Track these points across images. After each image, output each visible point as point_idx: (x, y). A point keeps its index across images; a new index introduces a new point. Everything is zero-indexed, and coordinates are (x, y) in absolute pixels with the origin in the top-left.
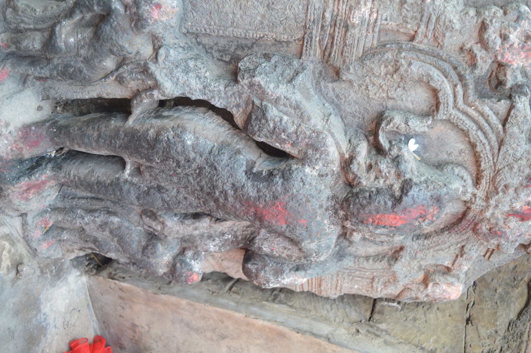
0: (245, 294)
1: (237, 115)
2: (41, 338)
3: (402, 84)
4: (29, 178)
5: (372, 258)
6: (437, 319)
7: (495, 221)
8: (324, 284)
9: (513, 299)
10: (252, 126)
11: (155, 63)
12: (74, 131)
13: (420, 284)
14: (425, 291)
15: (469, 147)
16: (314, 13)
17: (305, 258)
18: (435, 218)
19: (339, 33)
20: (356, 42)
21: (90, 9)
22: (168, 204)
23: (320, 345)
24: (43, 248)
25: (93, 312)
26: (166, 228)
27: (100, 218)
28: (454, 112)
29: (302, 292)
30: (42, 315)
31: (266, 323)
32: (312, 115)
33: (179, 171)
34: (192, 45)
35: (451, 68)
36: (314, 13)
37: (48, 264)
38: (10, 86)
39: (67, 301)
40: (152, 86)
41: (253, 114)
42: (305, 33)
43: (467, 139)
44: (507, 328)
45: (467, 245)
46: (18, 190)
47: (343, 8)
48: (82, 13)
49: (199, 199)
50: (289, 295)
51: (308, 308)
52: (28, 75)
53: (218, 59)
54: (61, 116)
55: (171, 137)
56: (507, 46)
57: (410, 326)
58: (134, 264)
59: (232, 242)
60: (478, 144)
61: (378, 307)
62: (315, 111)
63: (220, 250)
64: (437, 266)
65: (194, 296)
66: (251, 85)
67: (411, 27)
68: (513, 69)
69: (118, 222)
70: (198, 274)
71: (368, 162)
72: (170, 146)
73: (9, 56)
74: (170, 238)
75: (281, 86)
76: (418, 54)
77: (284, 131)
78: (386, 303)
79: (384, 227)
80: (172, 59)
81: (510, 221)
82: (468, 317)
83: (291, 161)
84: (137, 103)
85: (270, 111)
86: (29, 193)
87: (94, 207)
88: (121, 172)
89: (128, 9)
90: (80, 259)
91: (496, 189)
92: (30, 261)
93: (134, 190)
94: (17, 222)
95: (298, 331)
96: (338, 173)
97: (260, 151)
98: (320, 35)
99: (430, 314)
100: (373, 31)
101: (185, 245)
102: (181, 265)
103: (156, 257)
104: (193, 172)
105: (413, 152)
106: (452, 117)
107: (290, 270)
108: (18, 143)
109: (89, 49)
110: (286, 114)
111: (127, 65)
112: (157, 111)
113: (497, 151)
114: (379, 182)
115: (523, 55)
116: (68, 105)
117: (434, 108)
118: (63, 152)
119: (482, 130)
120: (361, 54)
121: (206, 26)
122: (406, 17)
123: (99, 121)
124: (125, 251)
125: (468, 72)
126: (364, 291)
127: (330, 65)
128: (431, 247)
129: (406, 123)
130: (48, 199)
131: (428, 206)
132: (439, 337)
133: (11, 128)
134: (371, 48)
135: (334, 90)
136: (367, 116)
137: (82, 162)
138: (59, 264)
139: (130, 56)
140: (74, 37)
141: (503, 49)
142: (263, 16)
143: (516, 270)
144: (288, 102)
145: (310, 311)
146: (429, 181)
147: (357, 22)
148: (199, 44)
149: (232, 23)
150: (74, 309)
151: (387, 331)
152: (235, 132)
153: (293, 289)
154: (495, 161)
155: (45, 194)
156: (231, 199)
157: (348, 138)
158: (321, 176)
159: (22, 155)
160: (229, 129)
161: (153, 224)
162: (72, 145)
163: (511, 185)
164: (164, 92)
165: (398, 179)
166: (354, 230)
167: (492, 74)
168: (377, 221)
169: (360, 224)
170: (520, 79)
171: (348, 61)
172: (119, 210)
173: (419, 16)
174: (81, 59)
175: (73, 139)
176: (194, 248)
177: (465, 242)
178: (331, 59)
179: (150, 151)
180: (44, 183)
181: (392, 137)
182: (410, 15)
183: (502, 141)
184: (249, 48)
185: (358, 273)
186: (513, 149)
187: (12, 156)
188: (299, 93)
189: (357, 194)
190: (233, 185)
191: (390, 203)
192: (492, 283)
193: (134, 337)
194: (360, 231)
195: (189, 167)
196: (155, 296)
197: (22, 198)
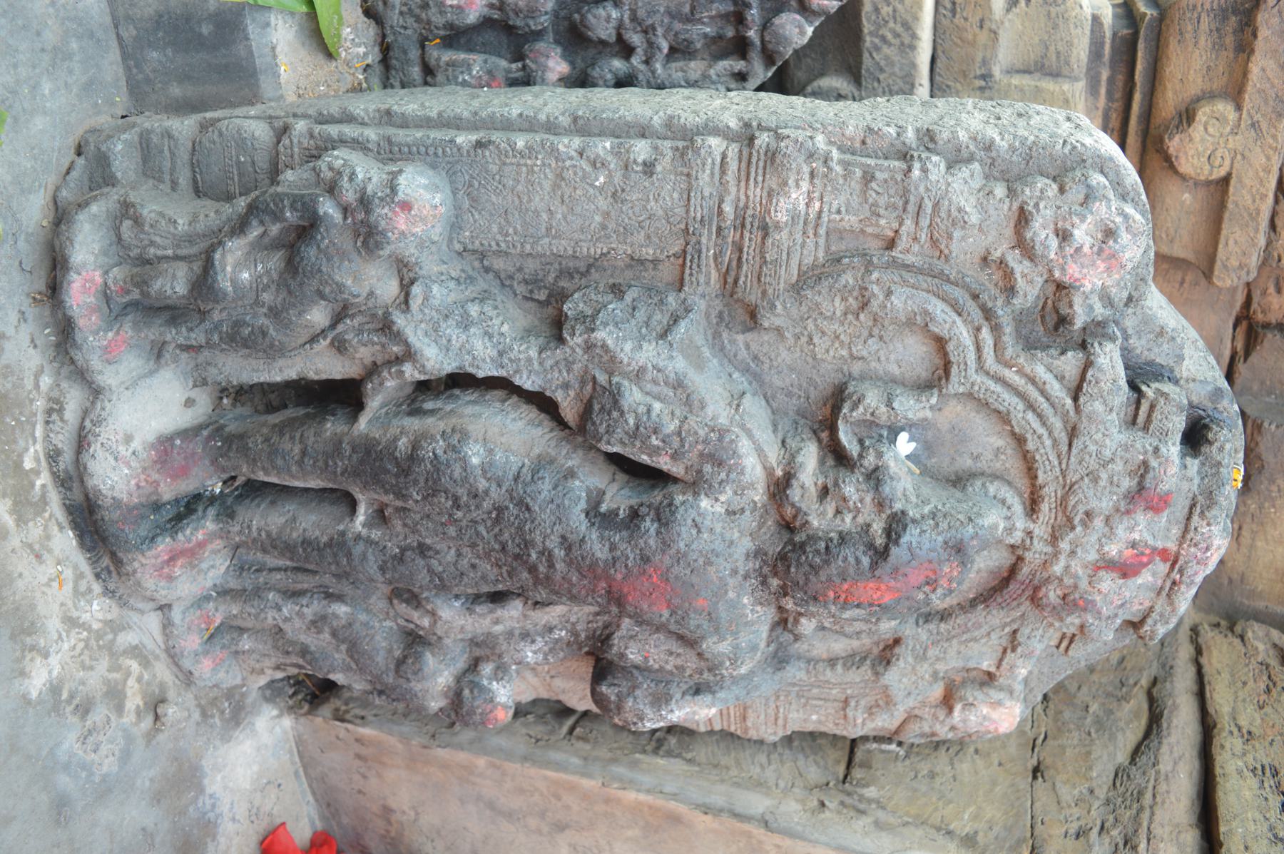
0: (600, 740)
1: (565, 404)
2: (206, 844)
3: (876, 331)
4: (172, 537)
5: (841, 662)
6: (976, 773)
9: (1122, 724)
10: (594, 424)
11: (403, 312)
12: (256, 443)
13: (936, 706)
14: (948, 720)
15: (1013, 444)
17: (710, 670)
19: (750, 240)
20: (784, 256)
21: (277, 216)
22: (441, 579)
23: (749, 835)
24: (204, 669)
25: (306, 785)
27: (313, 608)
28: (979, 379)
29: (711, 733)
30: (207, 798)
31: (642, 797)
32: (707, 397)
33: (459, 514)
34: (475, 274)
35: (967, 296)
37: (216, 698)
38: (133, 365)
39: (255, 768)
40: (400, 354)
42: (687, 244)
44: (1111, 782)
46: (153, 561)
47: (756, 193)
49: (500, 567)
50: (687, 738)
52: (164, 343)
53: (525, 298)
54: (231, 416)
55: (439, 452)
56: (1069, 250)
57: (924, 788)
58: (381, 693)
59: (569, 644)
60: (1029, 436)
61: (859, 755)
62: (714, 390)
64: (968, 670)
65: (501, 750)
66: (589, 347)
67: (886, 224)
69: (346, 613)
70: (505, 707)
71: (820, 482)
72: (438, 470)
73: (129, 309)
74: (447, 641)
75: (645, 345)
76: (904, 273)
77: (655, 432)
78: (875, 745)
79: (858, 606)
80: (436, 302)
81: (1101, 580)
82: (1035, 763)
83: (673, 488)
84: (373, 389)
85: (627, 394)
87: (299, 586)
88: (348, 519)
90: (277, 685)
91: (1070, 520)
92: (179, 694)
93: (374, 554)
94: (153, 621)
95: (706, 810)
96: (764, 506)
97: (613, 468)
98: (716, 245)
99: (961, 761)
100: (815, 235)
101: (478, 652)
102: (472, 691)
103: (423, 678)
104: (485, 516)
105: (908, 457)
106: (976, 388)
107: (684, 694)
109: (277, 291)
110: (658, 398)
111: (353, 317)
112: (413, 401)
113: (1066, 448)
114: (843, 520)
115: (1102, 266)
116: (241, 393)
117: (941, 372)
118: (236, 484)
119: (1034, 410)
120: (794, 278)
121: (499, 237)
122: (875, 204)
123: (303, 424)
124: (362, 670)
125: (999, 302)
127: (738, 301)
129: (889, 404)
130: (210, 574)
131: (940, 563)
132: (980, 808)
133: (136, 444)
134: (814, 267)
135: (748, 347)
136: (813, 394)
137: (273, 503)
138: (237, 697)
140: (249, 269)
141: (1063, 257)
142: (607, 215)
143: (1123, 666)
144: (660, 375)
145: (728, 768)
146: (939, 514)
147: (784, 219)
148: (487, 270)
149: (549, 229)
150: (269, 783)
151: (878, 802)
152: (563, 434)
153: (694, 727)
154: (1064, 466)
155: (204, 566)
156: (560, 566)
157: (780, 436)
159: (158, 494)
160: (551, 431)
161: (415, 615)
162: (253, 472)
164: (424, 366)
165: (880, 512)
166: (801, 614)
167: (1045, 303)
168: (843, 596)
170: (1100, 311)
171: (770, 291)
172: (347, 589)
173: (901, 204)
174: (265, 310)
175: (254, 460)
176: (495, 658)
179: (402, 480)
180: (201, 545)
181: (863, 432)
182: (882, 201)
183: (1074, 428)
184: (583, 275)
185: (815, 691)
186: (1097, 443)
187: (139, 497)
188: (680, 357)
189: (802, 546)
190: (563, 537)
191: (866, 561)
193: (388, 831)
194: (813, 615)
195: (477, 507)
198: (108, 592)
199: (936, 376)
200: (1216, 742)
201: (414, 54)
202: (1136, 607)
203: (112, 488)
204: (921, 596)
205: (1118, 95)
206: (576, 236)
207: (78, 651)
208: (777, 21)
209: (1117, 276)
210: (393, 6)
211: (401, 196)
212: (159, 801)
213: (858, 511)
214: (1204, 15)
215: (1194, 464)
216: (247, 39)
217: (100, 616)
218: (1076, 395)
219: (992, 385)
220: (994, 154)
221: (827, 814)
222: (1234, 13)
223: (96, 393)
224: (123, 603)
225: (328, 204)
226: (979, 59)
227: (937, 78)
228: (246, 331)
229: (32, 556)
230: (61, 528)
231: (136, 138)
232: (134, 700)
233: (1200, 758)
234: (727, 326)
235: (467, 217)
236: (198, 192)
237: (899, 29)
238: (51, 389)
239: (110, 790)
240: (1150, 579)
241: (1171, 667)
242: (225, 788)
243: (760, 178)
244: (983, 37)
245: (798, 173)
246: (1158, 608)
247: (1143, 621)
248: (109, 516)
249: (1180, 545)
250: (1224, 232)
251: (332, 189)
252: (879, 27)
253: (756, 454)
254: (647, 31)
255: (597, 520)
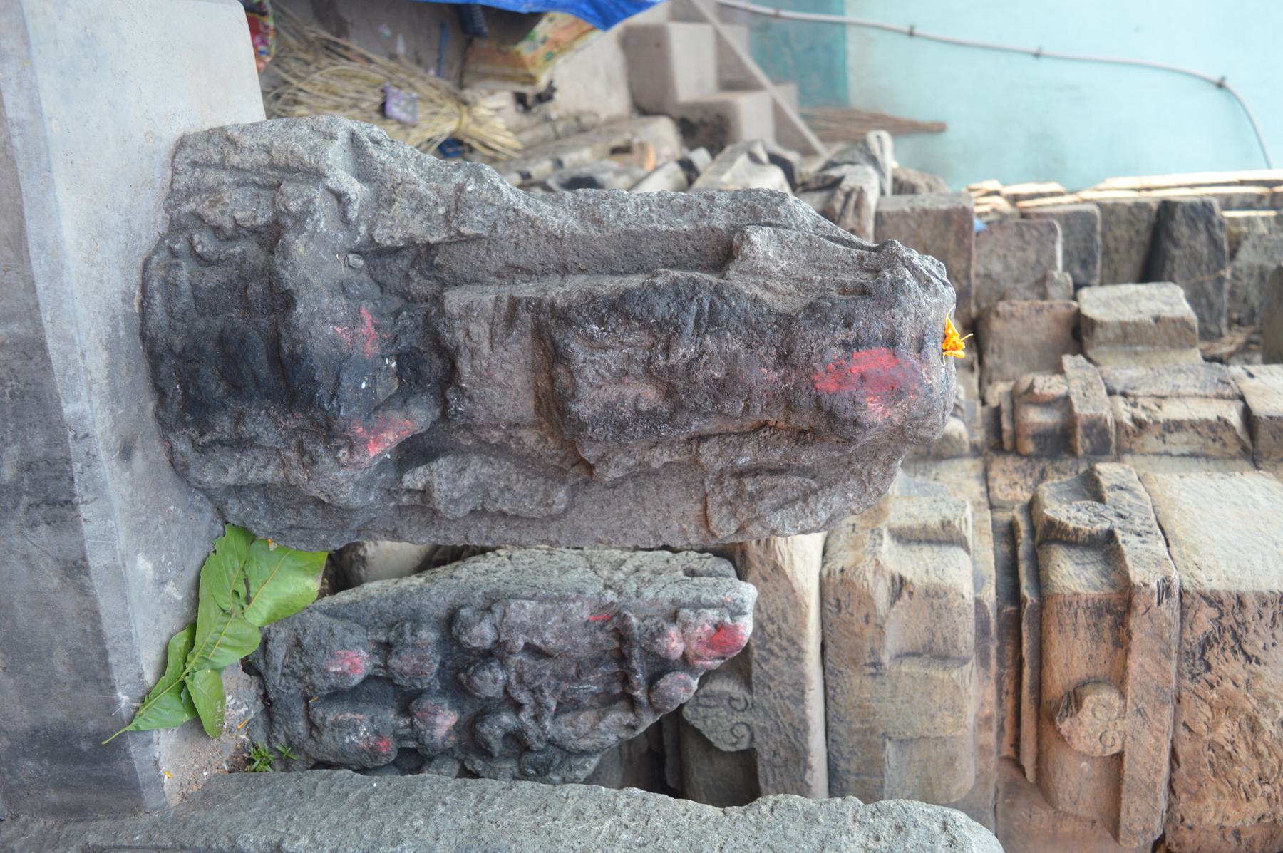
201: (299, 709)
205: (1009, 663)
208: (662, 683)
210: (276, 669)
214: (1080, 612)
216: (130, 758)
222: (1108, 611)
226: (867, 649)
227: (828, 664)
237: (785, 643)
244: (869, 631)
250: (1124, 802)
252: (765, 642)
254: (536, 691)
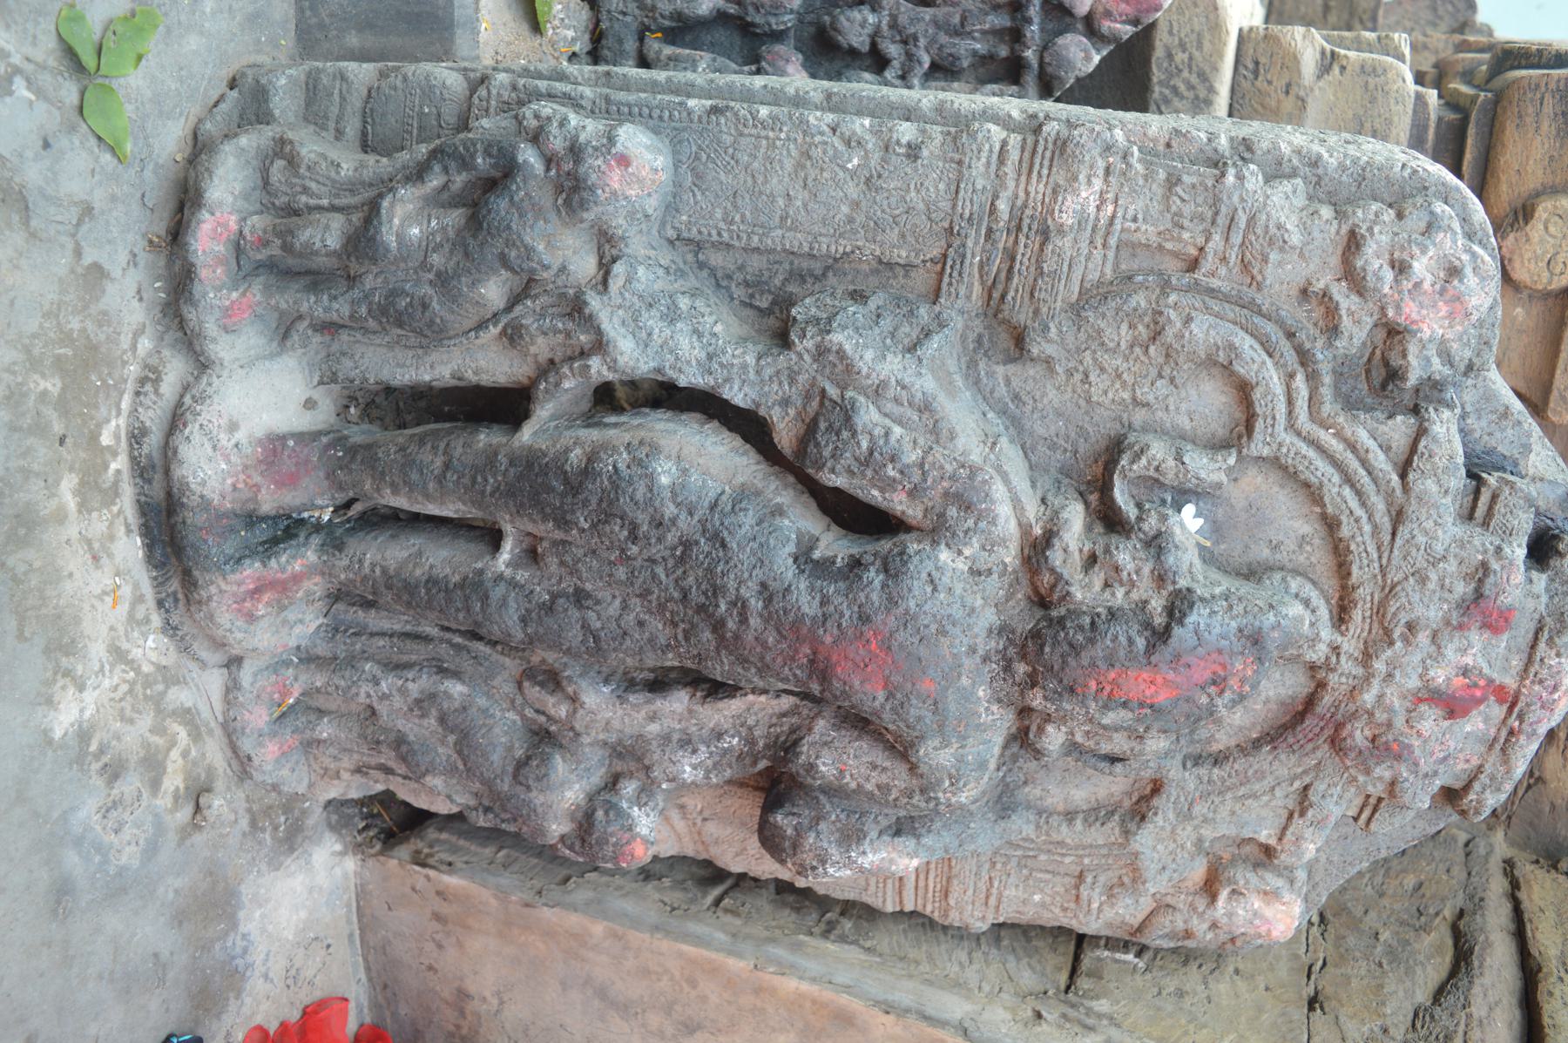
1: (782, 426)
3: (1167, 371)
5: (1081, 816)
6: (1237, 996)
7: (1385, 716)
8: (956, 888)
9: (1421, 958)
10: (817, 445)
11: (599, 293)
16: (971, 201)
17: (922, 791)
18: (1247, 688)
20: (1065, 268)
22: (597, 639)
26: (581, 712)
28: (1288, 438)
31: (805, 987)
32: (958, 428)
33: (634, 550)
34: (686, 268)
35: (1281, 334)
36: (971, 201)
37: (270, 807)
39: (303, 914)
40: (587, 347)
41: (822, 419)
43: (1318, 510)
44: (1409, 1024)
45: (1316, 784)
46: (235, 588)
47: (1038, 189)
48: (447, 173)
49: (675, 625)
50: (865, 924)
51: (911, 956)
56: (1407, 285)
57: (1169, 1008)
59: (740, 757)
60: (1344, 518)
63: (708, 778)
66: (821, 352)
67: (1190, 237)
68: (1421, 340)
69: (461, 694)
71: (1086, 549)
74: (586, 740)
77: (893, 459)
79: (1125, 705)
81: (1422, 717)
84: (547, 391)
86: (259, 600)
87: (405, 658)
89: (553, 165)
91: (1387, 632)
94: (215, 681)
96: (1014, 571)
98: (983, 251)
100: (1104, 246)
101: (619, 766)
102: (606, 813)
103: (548, 788)
106: (1284, 450)
108: (251, 471)
109: (451, 251)
114: (1113, 594)
117: (1242, 428)
119: (1353, 486)
121: (722, 225)
122: (1179, 214)
125: (1320, 343)
126: (1057, 911)
127: (1003, 321)
128: (1229, 788)
129: (1179, 458)
130: (298, 630)
131: (1232, 654)
134: (1100, 284)
135: (1008, 382)
136: (1083, 448)
137: (392, 536)
139: (545, 275)
140: (420, 224)
141: (1400, 292)
142: (856, 205)
144: (904, 393)
145: (917, 963)
147: (1070, 222)
148: (701, 265)
149: (783, 219)
150: (316, 939)
154: (1384, 561)
156: (754, 621)
157: (1039, 494)
158: (975, 572)
159: (256, 502)
162: (378, 490)
163: (1423, 622)
164: (615, 361)
167: (1373, 353)
168: (1108, 689)
169: (1066, 696)
171: (1044, 310)
172: (467, 665)
173: (1210, 214)
174: (431, 276)
176: (642, 775)
177: (1312, 774)
178: (1006, 307)
179: (569, 500)
180: (297, 579)
182: (1188, 210)
183: (1400, 513)
185: (1043, 857)
189: (1061, 622)
190: (764, 585)
191: (1141, 643)
192: (1367, 919)
193: (458, 1027)
194: (1063, 720)
195: (659, 540)
196: (526, 910)
197: (239, 611)
198: (170, 629)
199: (1235, 435)
200: (1542, 988)
202: (1461, 766)
203: (203, 483)
204: (1204, 700)
206: (816, 228)
207: (119, 694)
208: (1060, 41)
209: (1459, 328)
211: (619, 148)
212: (181, 923)
213: (1133, 584)
214: (1548, 96)
215: (1541, 580)
217: (153, 656)
218: (1404, 470)
219: (1304, 448)
220: (1320, 171)
221: (1045, 1026)
223: (202, 364)
224: (185, 649)
225: (529, 152)
228: (403, 303)
229: (88, 556)
230: (129, 531)
231: (303, 77)
232: (173, 781)
233: (1521, 1006)
234: (986, 354)
235: (687, 196)
236: (365, 147)
237: (1194, 79)
238: (150, 355)
239: (124, 890)
240: (1481, 726)
241: (1482, 900)
242: (263, 930)
243: (1045, 172)
245: (1091, 167)
246: (1488, 768)
247: (1467, 787)
248: (194, 518)
249: (1523, 679)
251: (536, 138)
252: (1171, 76)
253: (1012, 502)
254: (907, 41)
255: (808, 567)
